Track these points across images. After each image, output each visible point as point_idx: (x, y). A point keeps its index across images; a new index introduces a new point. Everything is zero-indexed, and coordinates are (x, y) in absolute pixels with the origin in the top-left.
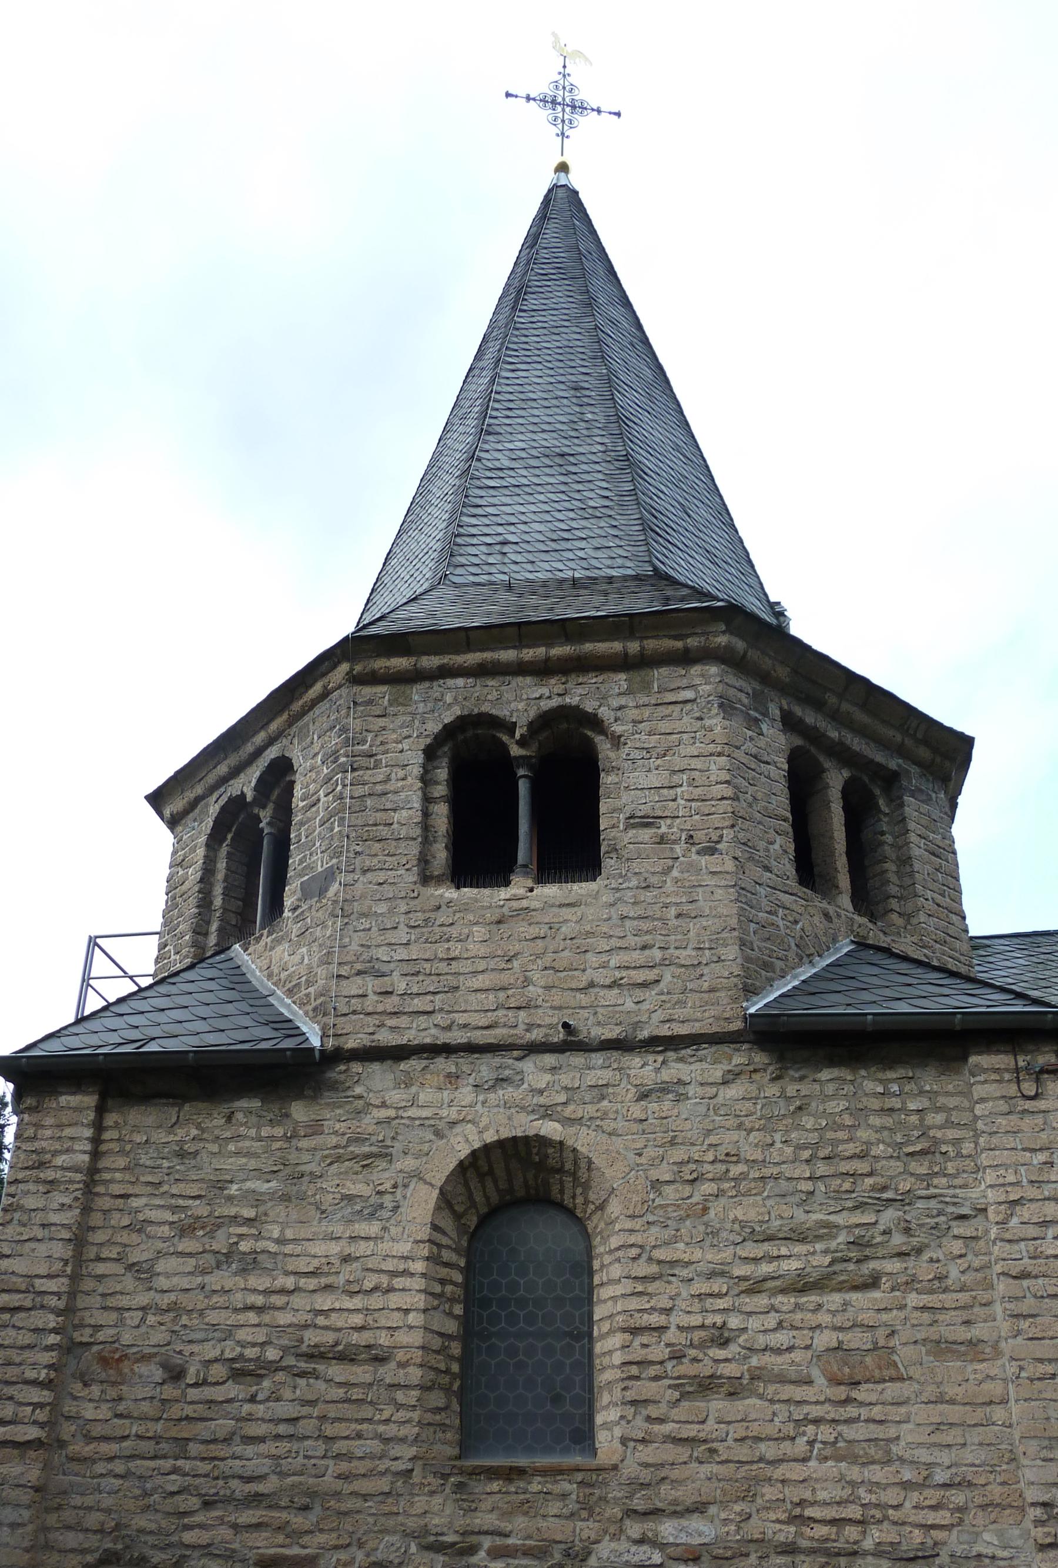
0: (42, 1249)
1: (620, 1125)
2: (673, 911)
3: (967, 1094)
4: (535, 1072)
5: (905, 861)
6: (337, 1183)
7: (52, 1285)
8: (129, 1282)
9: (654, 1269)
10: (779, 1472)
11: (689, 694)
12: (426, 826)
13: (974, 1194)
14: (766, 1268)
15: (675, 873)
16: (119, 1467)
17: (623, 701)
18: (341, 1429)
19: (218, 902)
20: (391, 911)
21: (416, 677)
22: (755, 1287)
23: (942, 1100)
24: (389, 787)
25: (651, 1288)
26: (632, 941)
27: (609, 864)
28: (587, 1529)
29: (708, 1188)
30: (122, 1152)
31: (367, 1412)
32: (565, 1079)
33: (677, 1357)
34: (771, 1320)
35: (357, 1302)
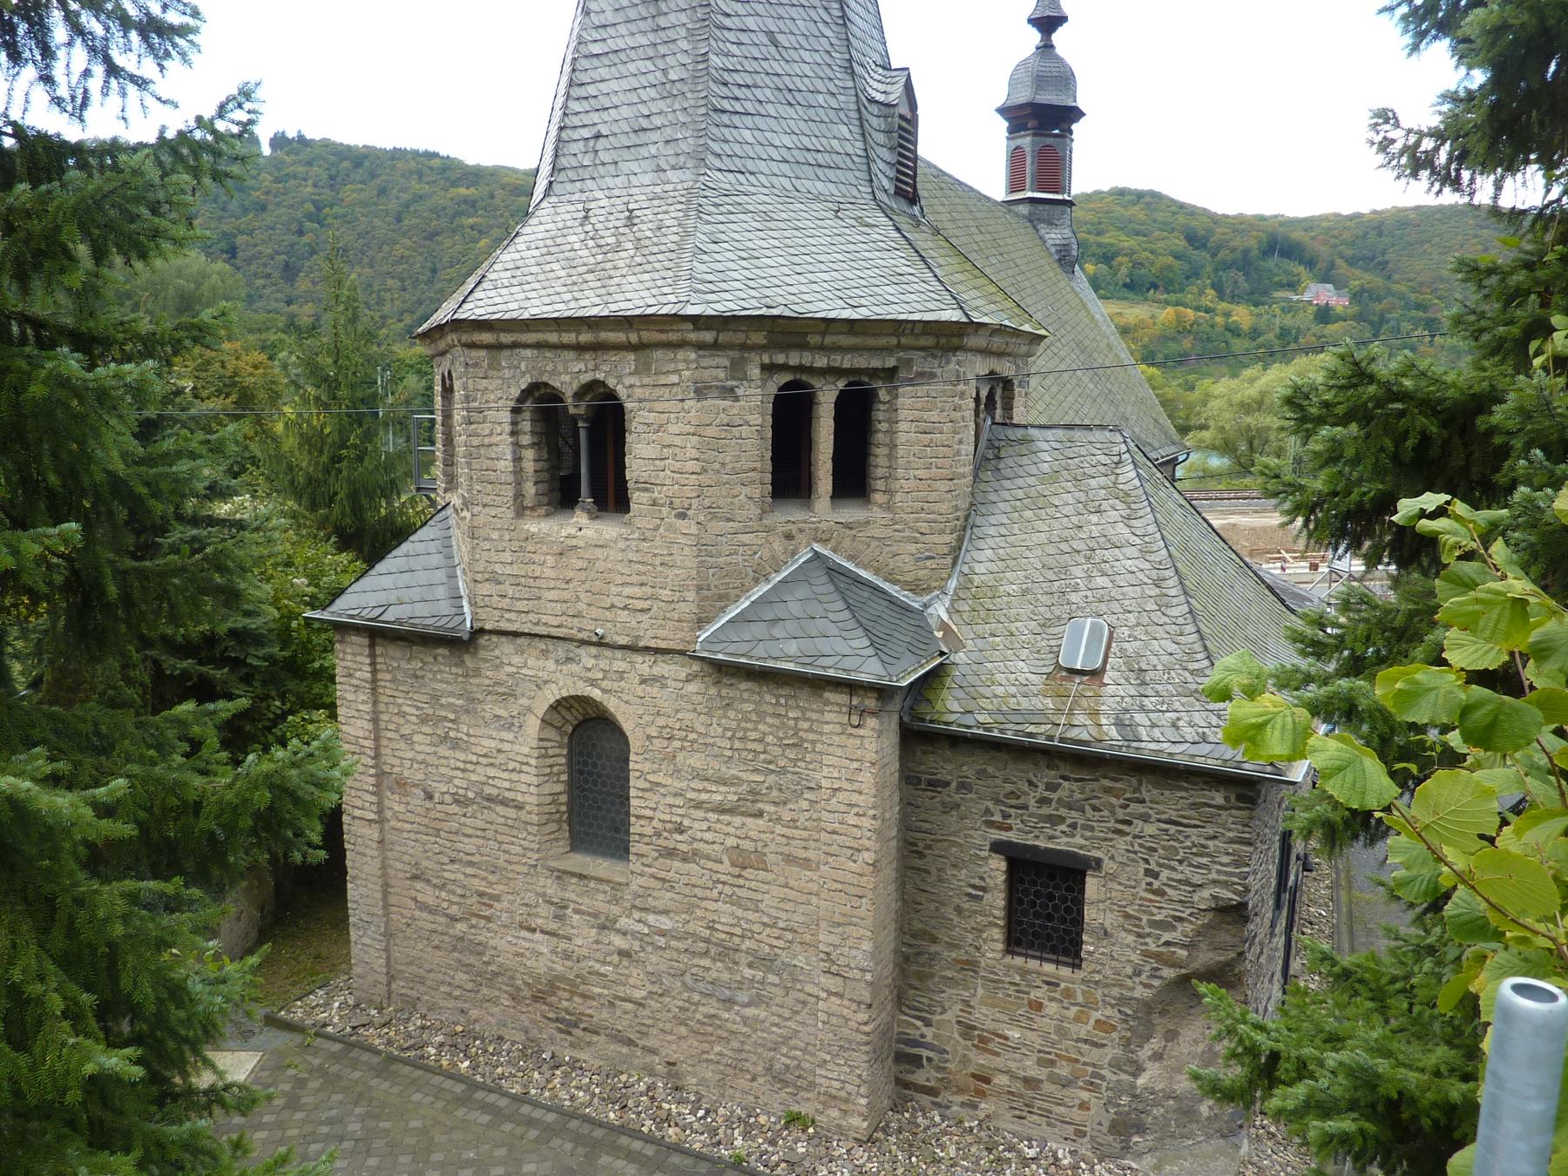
0: (359, 723)
2: (658, 561)
4: (587, 656)
5: (893, 446)
6: (491, 708)
8: (402, 745)
9: (647, 785)
10: (704, 904)
11: (674, 379)
12: (518, 472)
14: (704, 796)
15: (662, 530)
16: (412, 836)
21: (499, 347)
22: (698, 805)
23: (808, 714)
25: (647, 795)
26: (635, 579)
28: (616, 910)
29: (677, 744)
31: (515, 832)
32: (603, 664)
33: (658, 835)
34: (705, 826)
35: (505, 775)
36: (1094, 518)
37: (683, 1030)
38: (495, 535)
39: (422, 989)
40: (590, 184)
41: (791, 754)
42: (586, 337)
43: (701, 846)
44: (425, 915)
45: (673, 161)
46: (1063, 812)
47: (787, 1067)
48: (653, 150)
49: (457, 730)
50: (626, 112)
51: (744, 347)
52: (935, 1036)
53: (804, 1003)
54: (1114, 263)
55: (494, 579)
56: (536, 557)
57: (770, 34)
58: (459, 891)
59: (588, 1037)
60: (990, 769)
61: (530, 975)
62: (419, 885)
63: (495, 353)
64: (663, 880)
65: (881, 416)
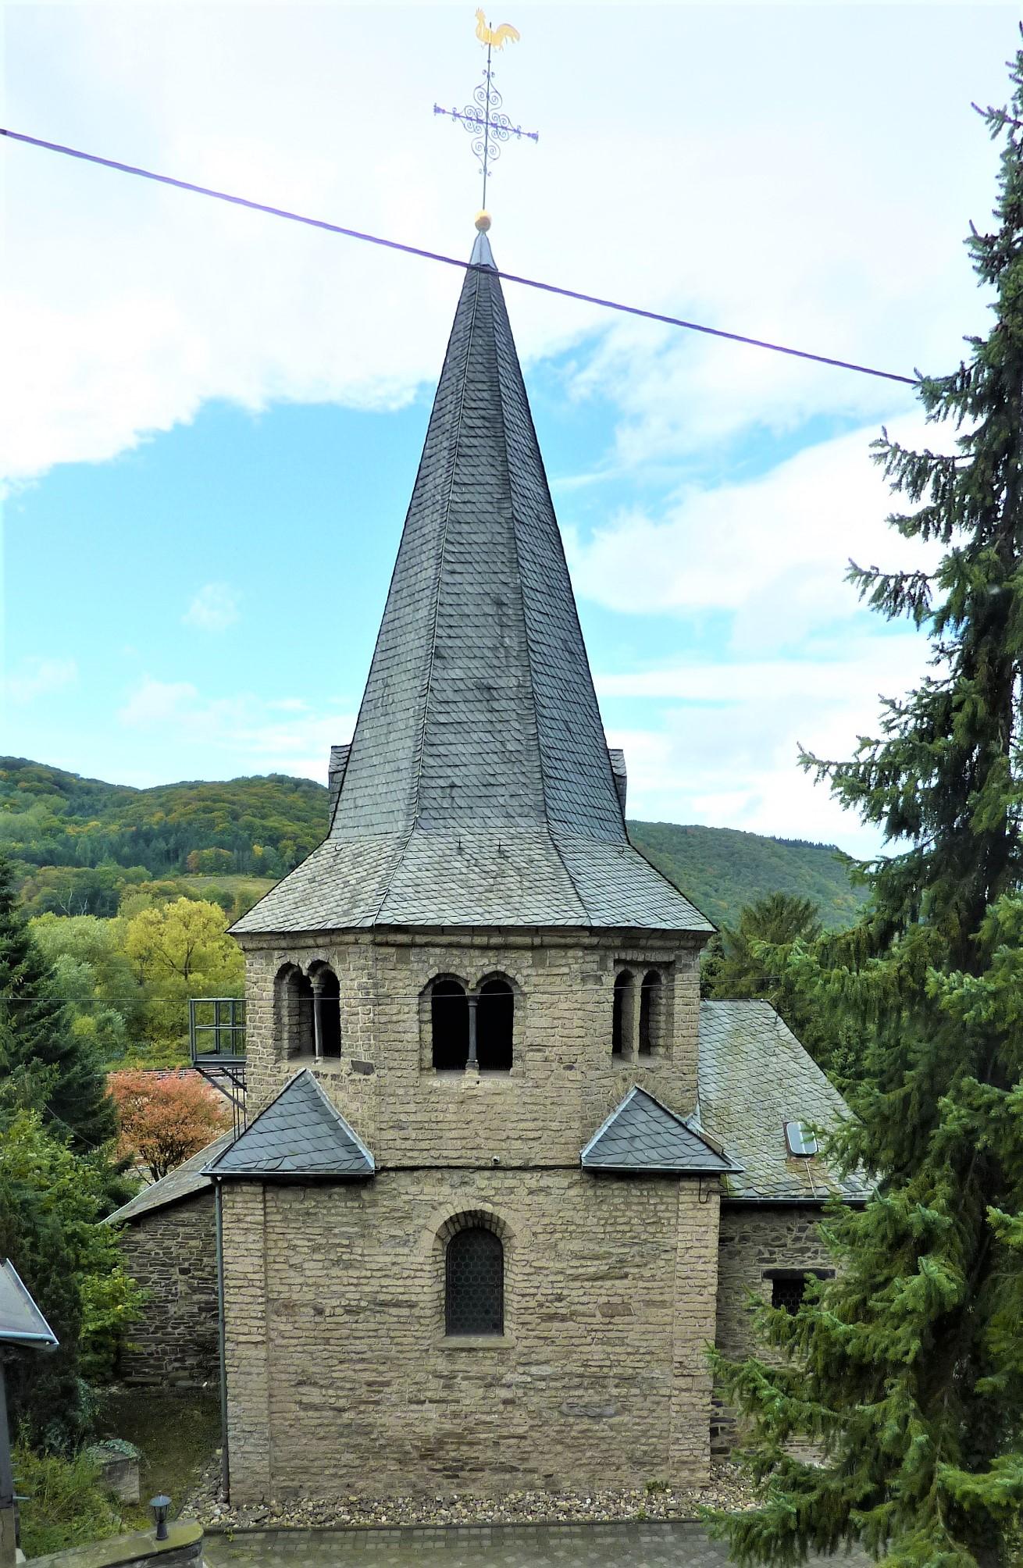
0: (248, 1260)
1: (520, 1207)
2: (549, 1101)
3: (677, 1197)
4: (480, 1180)
5: (670, 1015)
6: (386, 1230)
8: (292, 1273)
10: (581, 1349)
11: (565, 970)
13: (672, 1241)
14: (581, 1271)
16: (299, 1349)
18: (398, 1334)
19: (286, 1020)
20: (406, 1094)
21: (413, 945)
22: (576, 1278)
24: (401, 1017)
26: (528, 1116)
27: (517, 1065)
28: (502, 1370)
30: (278, 1212)
32: (495, 1183)
33: (541, 1305)
34: (581, 1292)
36: (774, 1059)
37: (559, 1448)
38: (401, 1091)
39: (304, 1477)
40: (451, 821)
41: (651, 1229)
42: (496, 940)
44: (310, 1413)
46: (809, 1244)
47: (645, 1452)
48: (501, 801)
49: (351, 1253)
53: (658, 1403)
54: (280, 845)
55: (399, 1126)
56: (439, 1106)
58: (348, 1386)
59: (474, 1475)
60: (762, 1224)
61: (419, 1439)
62: (304, 1389)
63: (403, 951)
64: (546, 1338)
65: (663, 994)
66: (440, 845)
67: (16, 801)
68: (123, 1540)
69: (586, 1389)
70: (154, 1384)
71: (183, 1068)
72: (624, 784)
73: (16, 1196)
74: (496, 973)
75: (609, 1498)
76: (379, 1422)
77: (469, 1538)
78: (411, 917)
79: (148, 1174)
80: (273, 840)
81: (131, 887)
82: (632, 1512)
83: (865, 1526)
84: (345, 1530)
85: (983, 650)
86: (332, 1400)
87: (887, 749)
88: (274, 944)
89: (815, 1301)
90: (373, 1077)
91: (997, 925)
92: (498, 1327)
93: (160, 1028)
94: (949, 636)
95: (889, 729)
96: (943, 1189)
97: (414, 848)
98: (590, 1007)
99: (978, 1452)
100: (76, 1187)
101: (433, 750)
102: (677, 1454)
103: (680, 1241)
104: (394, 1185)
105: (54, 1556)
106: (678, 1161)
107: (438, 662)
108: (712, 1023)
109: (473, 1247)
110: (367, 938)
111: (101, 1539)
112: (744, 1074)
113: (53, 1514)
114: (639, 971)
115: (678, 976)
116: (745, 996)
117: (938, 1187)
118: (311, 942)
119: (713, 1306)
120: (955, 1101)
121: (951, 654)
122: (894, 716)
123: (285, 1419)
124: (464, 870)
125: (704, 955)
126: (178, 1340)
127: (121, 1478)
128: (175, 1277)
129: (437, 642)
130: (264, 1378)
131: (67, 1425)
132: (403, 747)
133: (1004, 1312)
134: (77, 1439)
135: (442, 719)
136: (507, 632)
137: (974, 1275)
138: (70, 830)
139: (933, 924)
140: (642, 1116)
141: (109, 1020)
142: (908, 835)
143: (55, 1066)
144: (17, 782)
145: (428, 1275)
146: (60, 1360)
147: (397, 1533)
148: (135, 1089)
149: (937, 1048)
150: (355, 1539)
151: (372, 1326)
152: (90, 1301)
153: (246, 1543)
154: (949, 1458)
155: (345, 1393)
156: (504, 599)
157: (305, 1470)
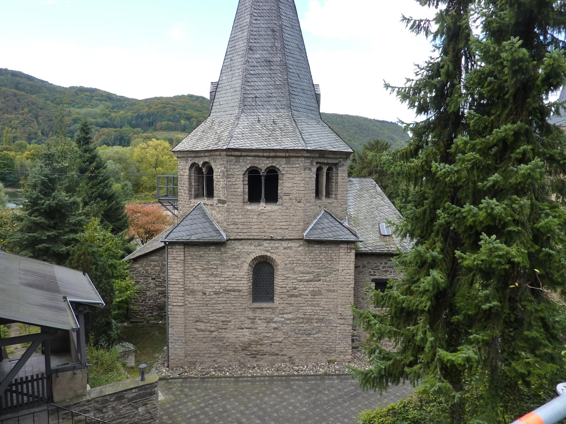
0: (178, 274)
1: (280, 254)
2: (292, 214)
4: (266, 244)
5: (337, 183)
6: (231, 262)
7: (181, 280)
8: (194, 279)
11: (298, 165)
13: (337, 267)
14: (303, 278)
16: (197, 308)
17: (284, 166)
19: (193, 184)
20: (238, 212)
21: (241, 156)
22: (301, 281)
24: (236, 183)
26: (284, 220)
28: (273, 316)
29: (295, 265)
30: (189, 256)
31: (238, 299)
32: (271, 245)
33: (288, 291)
34: (303, 286)
35: (235, 282)
36: (375, 200)
37: (295, 346)
38: (236, 211)
39: (198, 357)
41: (329, 263)
42: (272, 154)
43: (302, 292)
44: (200, 333)
45: (281, 107)
46: (388, 269)
50: (264, 91)
51: (313, 158)
52: (357, 333)
53: (332, 329)
54: (191, 121)
56: (250, 216)
57: (298, 74)
58: (215, 322)
59: (262, 357)
62: (198, 324)
63: (238, 158)
64: (290, 304)
66: (252, 119)
67: (93, 104)
68: (128, 381)
69: (305, 324)
70: (141, 322)
71: (154, 203)
72: (320, 97)
73: (90, 250)
74: (272, 166)
75: (313, 366)
76: (227, 336)
77: (260, 381)
78: (241, 146)
79: (140, 243)
80: (188, 118)
81: (135, 135)
82: (322, 371)
83: (410, 373)
84: (213, 378)
85: (451, 47)
86: (209, 328)
87: (416, 83)
88: (189, 155)
89: (391, 287)
90: (226, 205)
91: (457, 146)
92: (272, 300)
93: (145, 188)
94: (438, 41)
95: (417, 75)
96: (439, 245)
97: (242, 120)
98: (307, 179)
99: (453, 346)
100: (113, 247)
101: (249, 84)
102: (339, 349)
103: (340, 267)
104: (233, 246)
105: (101, 387)
106: (340, 237)
107: (251, 52)
108: (352, 186)
109: (263, 270)
110: (224, 153)
111: (120, 381)
112: (364, 205)
113: (101, 371)
114: (325, 167)
115: (340, 168)
116: (364, 177)
117: (437, 244)
118: (203, 155)
119: (352, 292)
120: (443, 212)
121: (439, 48)
122: (419, 70)
123: (190, 335)
124: (260, 128)
125: (349, 162)
126: (150, 305)
127: (128, 357)
128: (149, 281)
129: (250, 44)
130: (183, 319)
131: (108, 337)
132: (238, 83)
133: (462, 291)
134: (111, 342)
135: (252, 72)
136: (276, 41)
137: (450, 278)
138: (113, 115)
139: (434, 146)
140: (326, 221)
141: (126, 185)
142: (424, 114)
143: (106, 201)
144: (93, 97)
145: (246, 279)
146: (105, 312)
147: (233, 379)
148: (135, 210)
149: (436, 192)
150: (217, 381)
151: (224, 299)
152: (117, 290)
153: (175, 383)
154: (442, 347)
155: (214, 325)
156: (275, 29)
157: (198, 355)
